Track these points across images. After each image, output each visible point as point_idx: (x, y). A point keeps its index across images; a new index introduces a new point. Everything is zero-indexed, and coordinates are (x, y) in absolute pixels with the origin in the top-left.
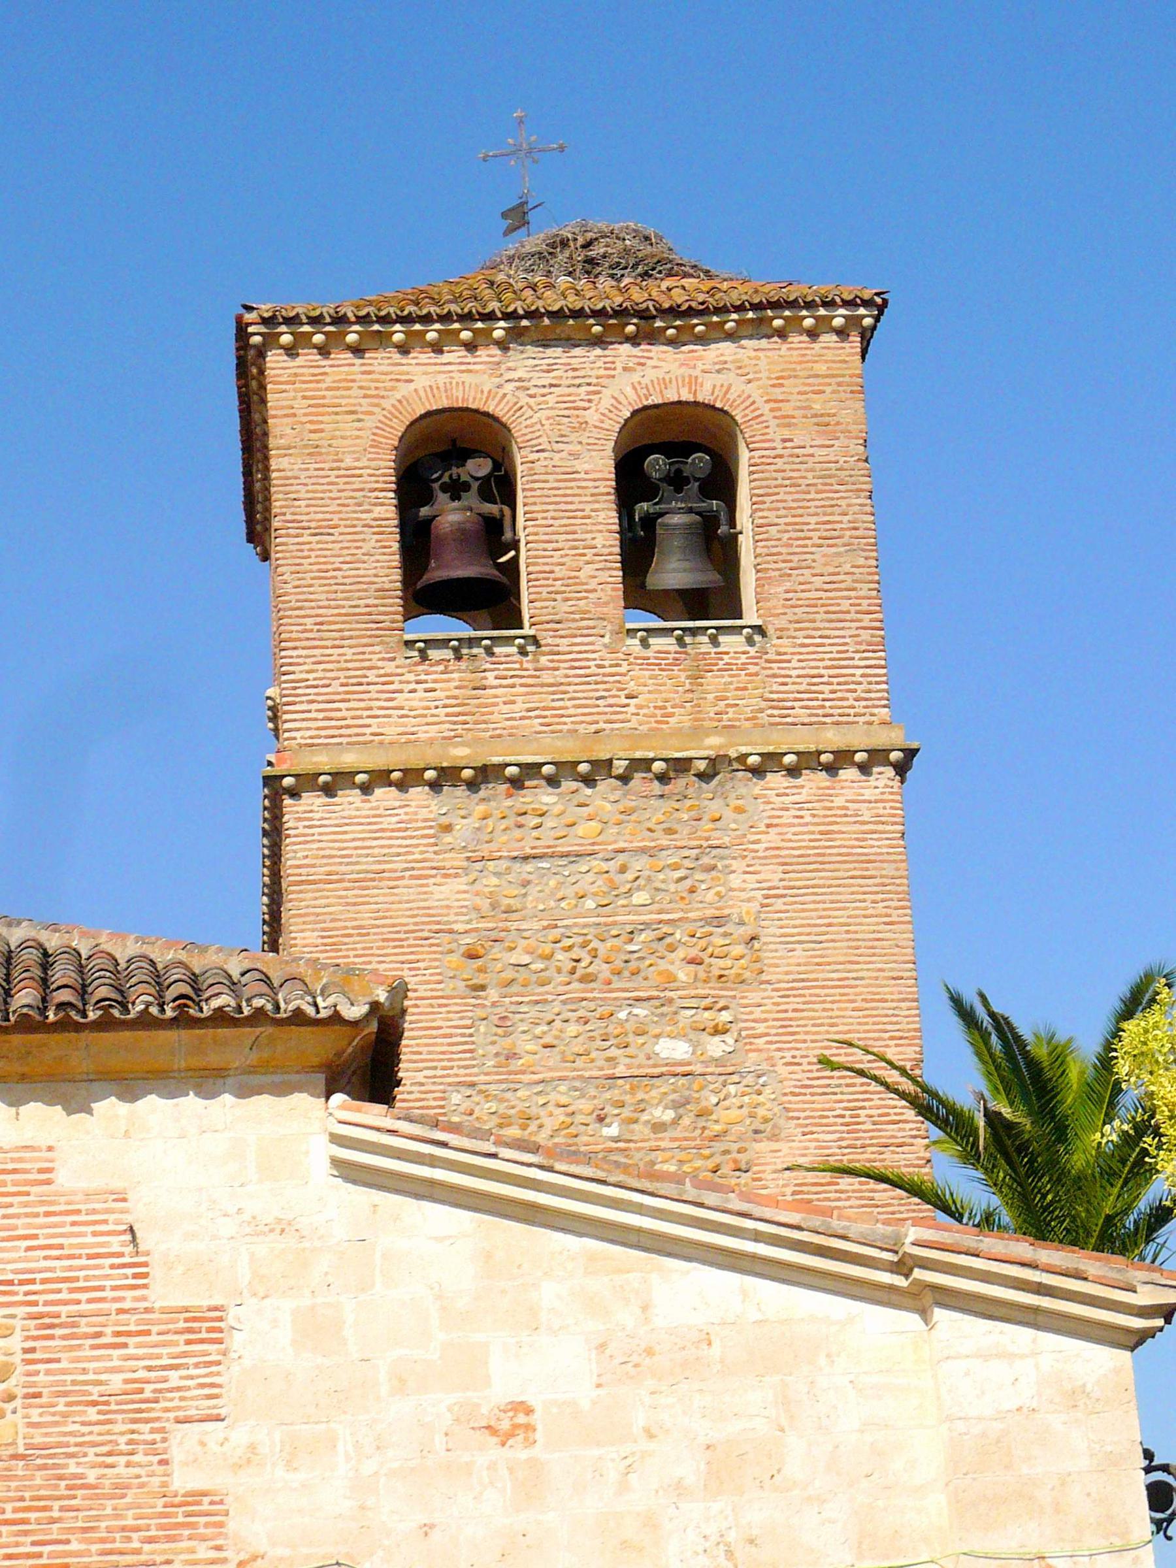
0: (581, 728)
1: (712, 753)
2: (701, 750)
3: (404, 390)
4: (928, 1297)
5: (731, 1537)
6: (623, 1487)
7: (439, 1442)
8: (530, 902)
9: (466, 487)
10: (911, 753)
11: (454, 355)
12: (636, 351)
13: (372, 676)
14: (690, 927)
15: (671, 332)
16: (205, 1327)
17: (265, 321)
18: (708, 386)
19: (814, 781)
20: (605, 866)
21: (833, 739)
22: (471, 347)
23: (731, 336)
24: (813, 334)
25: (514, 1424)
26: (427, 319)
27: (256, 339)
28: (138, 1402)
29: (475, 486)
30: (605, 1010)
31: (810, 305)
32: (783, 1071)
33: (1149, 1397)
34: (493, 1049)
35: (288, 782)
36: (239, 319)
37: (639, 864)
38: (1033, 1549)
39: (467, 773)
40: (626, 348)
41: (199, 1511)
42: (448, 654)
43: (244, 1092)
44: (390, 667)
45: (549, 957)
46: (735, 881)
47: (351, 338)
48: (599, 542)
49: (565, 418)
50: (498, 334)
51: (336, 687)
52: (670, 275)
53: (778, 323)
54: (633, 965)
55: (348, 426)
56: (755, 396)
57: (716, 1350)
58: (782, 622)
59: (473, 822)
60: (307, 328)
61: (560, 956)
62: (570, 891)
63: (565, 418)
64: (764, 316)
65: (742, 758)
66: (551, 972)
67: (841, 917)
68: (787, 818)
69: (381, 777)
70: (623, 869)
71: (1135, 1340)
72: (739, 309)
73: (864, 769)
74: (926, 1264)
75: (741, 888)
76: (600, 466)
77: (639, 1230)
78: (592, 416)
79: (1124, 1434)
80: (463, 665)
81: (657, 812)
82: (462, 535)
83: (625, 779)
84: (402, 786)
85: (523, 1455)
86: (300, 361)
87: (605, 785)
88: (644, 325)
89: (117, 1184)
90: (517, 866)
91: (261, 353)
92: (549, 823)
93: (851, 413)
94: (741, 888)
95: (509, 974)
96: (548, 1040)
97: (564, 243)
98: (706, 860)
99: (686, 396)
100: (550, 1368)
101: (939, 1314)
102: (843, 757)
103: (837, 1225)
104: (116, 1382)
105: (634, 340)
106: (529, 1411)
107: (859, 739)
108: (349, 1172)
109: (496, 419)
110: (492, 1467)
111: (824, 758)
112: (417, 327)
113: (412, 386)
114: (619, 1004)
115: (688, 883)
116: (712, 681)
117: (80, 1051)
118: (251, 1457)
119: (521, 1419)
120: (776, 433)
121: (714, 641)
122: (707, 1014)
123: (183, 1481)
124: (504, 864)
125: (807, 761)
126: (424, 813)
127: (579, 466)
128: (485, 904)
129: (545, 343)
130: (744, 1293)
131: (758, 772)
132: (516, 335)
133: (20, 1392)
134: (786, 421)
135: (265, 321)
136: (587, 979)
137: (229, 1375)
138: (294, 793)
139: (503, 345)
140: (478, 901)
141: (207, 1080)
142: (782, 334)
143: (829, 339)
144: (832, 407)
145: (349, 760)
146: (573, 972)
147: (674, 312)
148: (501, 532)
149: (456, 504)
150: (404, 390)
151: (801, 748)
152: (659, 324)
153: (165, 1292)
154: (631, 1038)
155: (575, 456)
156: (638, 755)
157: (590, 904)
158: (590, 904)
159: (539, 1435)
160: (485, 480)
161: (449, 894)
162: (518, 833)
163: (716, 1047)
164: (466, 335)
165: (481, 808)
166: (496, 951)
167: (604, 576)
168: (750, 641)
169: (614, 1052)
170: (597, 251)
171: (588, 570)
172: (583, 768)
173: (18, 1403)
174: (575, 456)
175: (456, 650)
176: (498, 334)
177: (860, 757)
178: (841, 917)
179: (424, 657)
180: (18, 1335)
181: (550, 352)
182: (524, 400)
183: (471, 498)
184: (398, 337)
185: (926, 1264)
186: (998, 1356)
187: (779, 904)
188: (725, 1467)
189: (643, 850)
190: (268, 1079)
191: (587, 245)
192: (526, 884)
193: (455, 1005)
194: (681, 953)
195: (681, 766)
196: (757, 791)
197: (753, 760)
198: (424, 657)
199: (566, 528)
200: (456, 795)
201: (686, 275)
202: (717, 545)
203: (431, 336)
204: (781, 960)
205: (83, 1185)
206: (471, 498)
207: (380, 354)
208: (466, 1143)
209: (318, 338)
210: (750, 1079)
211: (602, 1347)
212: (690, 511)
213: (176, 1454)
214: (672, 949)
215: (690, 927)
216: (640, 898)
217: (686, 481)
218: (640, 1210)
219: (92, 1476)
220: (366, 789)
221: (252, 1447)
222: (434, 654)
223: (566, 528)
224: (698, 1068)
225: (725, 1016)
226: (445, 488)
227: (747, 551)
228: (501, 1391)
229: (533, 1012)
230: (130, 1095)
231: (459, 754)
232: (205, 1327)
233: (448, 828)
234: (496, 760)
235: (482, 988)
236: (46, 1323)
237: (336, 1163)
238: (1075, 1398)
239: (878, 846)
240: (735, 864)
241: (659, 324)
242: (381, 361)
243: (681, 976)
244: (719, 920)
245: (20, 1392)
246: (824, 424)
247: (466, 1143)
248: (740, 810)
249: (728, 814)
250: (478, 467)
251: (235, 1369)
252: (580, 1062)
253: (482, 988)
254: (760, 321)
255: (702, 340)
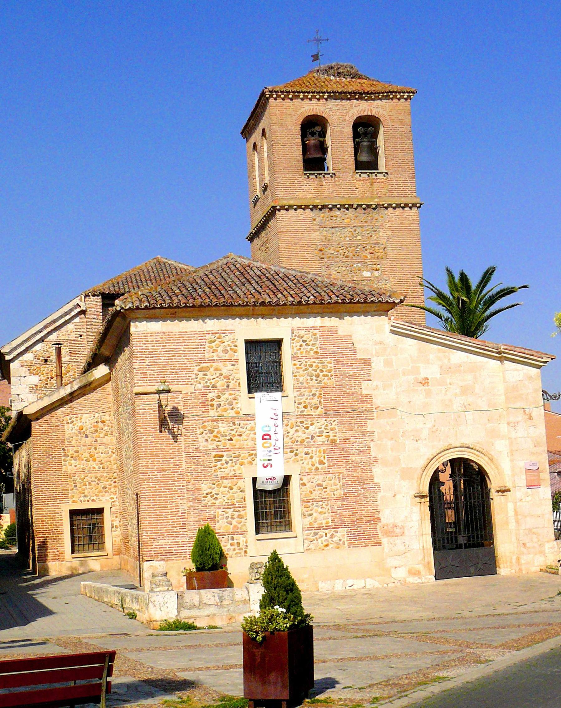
0: (345, 196)
1: (376, 203)
2: (373, 203)
3: (303, 110)
4: (503, 358)
5: (466, 404)
6: (446, 394)
7: (412, 385)
8: (334, 238)
9: (315, 134)
10: (421, 204)
11: (314, 101)
12: (358, 102)
13: (296, 181)
14: (371, 245)
15: (366, 98)
16: (367, 362)
17: (270, 92)
18: (374, 111)
19: (399, 210)
20: (351, 230)
21: (403, 201)
22: (319, 99)
23: (380, 99)
24: (399, 99)
25: (425, 382)
26: (309, 93)
27: (268, 96)
28: (355, 377)
29: (317, 133)
30: (351, 264)
31: (399, 93)
32: (392, 280)
33: (544, 378)
34: (326, 273)
35: (278, 207)
36: (263, 90)
37: (359, 229)
38: (522, 407)
39: (320, 207)
40: (355, 101)
41: (368, 398)
42: (314, 177)
43: (372, 316)
44: (300, 179)
45: (338, 251)
46: (381, 234)
47: (290, 96)
48: (349, 150)
49: (341, 117)
50: (325, 97)
51: (288, 184)
52: (359, 78)
53: (391, 96)
54: (357, 254)
55: (289, 119)
56: (386, 114)
57: (462, 368)
58: (391, 171)
59: (321, 218)
60: (280, 94)
61: (341, 251)
62: (343, 236)
63: (341, 117)
64: (388, 95)
65: (383, 205)
66: (339, 255)
67: (405, 243)
68: (393, 219)
69: (300, 207)
70: (355, 231)
71: (539, 367)
72: (383, 93)
73: (411, 208)
74: (504, 353)
75: (382, 235)
76: (349, 130)
77: (449, 345)
78: (347, 118)
79: (538, 385)
80: (318, 179)
81: (362, 217)
82: (315, 146)
83: (356, 209)
84: (304, 209)
85: (427, 388)
86: (277, 101)
87: (351, 210)
88: (359, 95)
89: (350, 334)
90: (331, 229)
91: (268, 99)
92: (338, 219)
93: (408, 119)
94: (382, 235)
95: (329, 255)
96: (338, 271)
97: (332, 68)
98: (374, 229)
99: (369, 114)
100: (431, 371)
101: (505, 362)
102: (406, 205)
103: (487, 344)
104: (351, 373)
105: (357, 99)
106: (428, 379)
107: (410, 201)
108: (393, 332)
109: (324, 118)
110: (421, 390)
111: (402, 205)
112: (306, 94)
113: (304, 109)
114: (354, 263)
115: (370, 234)
116: (376, 185)
117: (343, 308)
118: (377, 388)
119: (427, 381)
120: (390, 124)
121: (376, 175)
122: (375, 266)
123: (364, 392)
124: (327, 229)
125: (398, 206)
126: (309, 216)
127: (343, 130)
128: (324, 238)
129: (336, 99)
130: (467, 356)
131: (386, 208)
132: (330, 97)
133: (333, 375)
134: (393, 121)
135: (270, 92)
136: (347, 257)
137: (372, 372)
138: (279, 210)
139: (326, 99)
140: (322, 237)
141: (366, 313)
142: (392, 99)
143: (403, 100)
144: (403, 118)
145: (292, 202)
146: (344, 255)
147: (368, 93)
148: (324, 145)
149: (313, 138)
150: (303, 110)
151: (397, 203)
152: (364, 96)
153: (360, 356)
154: (357, 271)
155: (343, 128)
156: (360, 203)
157: (348, 239)
158: (348, 239)
159: (430, 384)
160: (320, 132)
161: (315, 235)
162: (331, 221)
163: (376, 274)
164: (318, 97)
165: (322, 215)
166: (326, 250)
167: (350, 158)
168: (384, 176)
169: (353, 274)
170: (341, 70)
171: (347, 157)
172: (347, 206)
173: (333, 377)
174: (343, 128)
175: (316, 176)
176: (325, 97)
177: (410, 205)
178: (405, 243)
179: (308, 177)
180: (333, 364)
181: (337, 101)
182: (331, 113)
183: (316, 136)
184: (301, 96)
185: (504, 353)
186: (516, 370)
187: (391, 240)
188: (465, 390)
189: (360, 226)
190: (377, 313)
191: (338, 69)
192: (333, 233)
193: (317, 262)
194: (368, 251)
195: (369, 206)
196: (386, 212)
197: (386, 205)
198: (308, 177)
199: (339, 144)
200: (316, 211)
201: (363, 79)
202: (374, 151)
203: (310, 96)
204: (392, 253)
205: (343, 334)
206: (316, 136)
207: (297, 100)
208: (417, 327)
209: (282, 96)
210: (384, 281)
211: (441, 367)
212: (368, 142)
213: (363, 387)
214: (366, 250)
215: (371, 245)
216: (359, 238)
217: (368, 134)
218: (450, 341)
219: (348, 391)
220: (296, 210)
221: (377, 386)
222: (311, 176)
223: (339, 144)
224: (372, 279)
225: (379, 266)
226: (310, 134)
227: (382, 152)
228: (423, 376)
229: (335, 264)
230: (351, 316)
231: (317, 202)
232: (367, 362)
233: (315, 220)
234: (327, 204)
235: (323, 258)
236: (338, 362)
237: (391, 330)
238: (530, 378)
239: (413, 227)
240: (381, 230)
241: (364, 96)
242: (297, 102)
243: (369, 257)
244: (377, 244)
245: (333, 375)
246: (401, 122)
247: (417, 327)
248: (382, 217)
249: (379, 218)
250: (318, 129)
251: (373, 370)
252: (346, 277)
253: (323, 258)
254: (387, 96)
255: (373, 100)
